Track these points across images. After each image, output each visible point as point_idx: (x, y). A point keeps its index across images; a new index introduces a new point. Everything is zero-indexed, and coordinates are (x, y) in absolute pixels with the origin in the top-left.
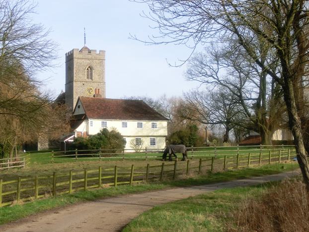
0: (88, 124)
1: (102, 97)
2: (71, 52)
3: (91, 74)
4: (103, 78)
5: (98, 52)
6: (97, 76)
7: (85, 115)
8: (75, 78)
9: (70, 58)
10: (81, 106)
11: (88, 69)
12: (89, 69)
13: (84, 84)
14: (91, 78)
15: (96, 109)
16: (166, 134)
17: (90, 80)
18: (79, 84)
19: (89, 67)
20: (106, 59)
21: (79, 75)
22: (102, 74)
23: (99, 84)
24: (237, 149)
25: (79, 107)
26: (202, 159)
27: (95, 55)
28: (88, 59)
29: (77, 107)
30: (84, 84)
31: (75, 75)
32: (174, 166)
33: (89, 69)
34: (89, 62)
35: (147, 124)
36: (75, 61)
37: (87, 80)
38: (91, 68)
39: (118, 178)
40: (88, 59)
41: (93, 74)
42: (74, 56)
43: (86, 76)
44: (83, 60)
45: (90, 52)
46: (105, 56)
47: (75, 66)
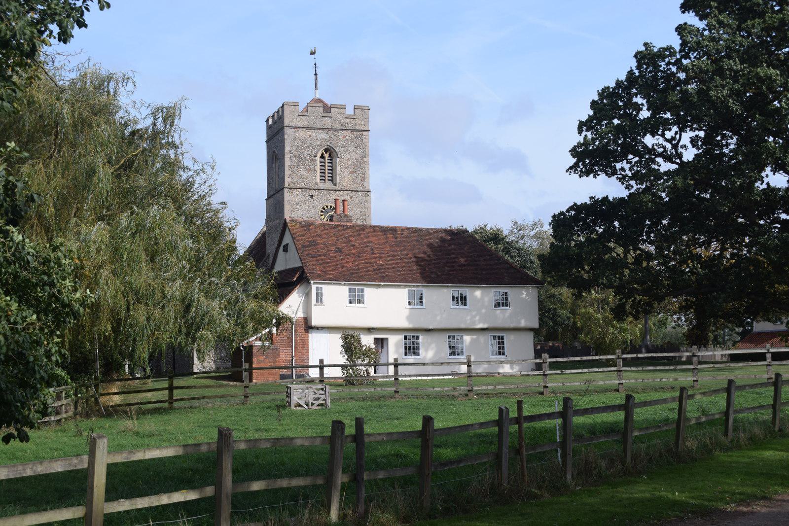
0: (308, 295)
1: (357, 221)
2: (278, 112)
3: (332, 169)
4: (363, 179)
5: (349, 111)
6: (346, 173)
7: (301, 270)
8: (287, 180)
9: (276, 131)
10: (292, 247)
11: (322, 157)
12: (327, 156)
13: (312, 196)
14: (332, 180)
15: (332, 254)
16: (536, 325)
17: (329, 185)
18: (300, 196)
19: (326, 151)
20: (371, 126)
21: (300, 172)
22: (360, 169)
23: (354, 194)
24: (765, 360)
25: (286, 249)
26: (638, 398)
27: (340, 118)
28: (323, 129)
29: (281, 248)
30: (312, 196)
31: (287, 172)
32: (770, 411)
33: (327, 156)
34: (323, 135)
35: (480, 296)
36: (289, 134)
37: (322, 185)
38: (330, 152)
39: (112, 470)
40: (323, 129)
41: (338, 168)
42: (287, 121)
43: (319, 174)
44: (310, 132)
45: (327, 109)
46: (539, 314)
47: (287, 148)
